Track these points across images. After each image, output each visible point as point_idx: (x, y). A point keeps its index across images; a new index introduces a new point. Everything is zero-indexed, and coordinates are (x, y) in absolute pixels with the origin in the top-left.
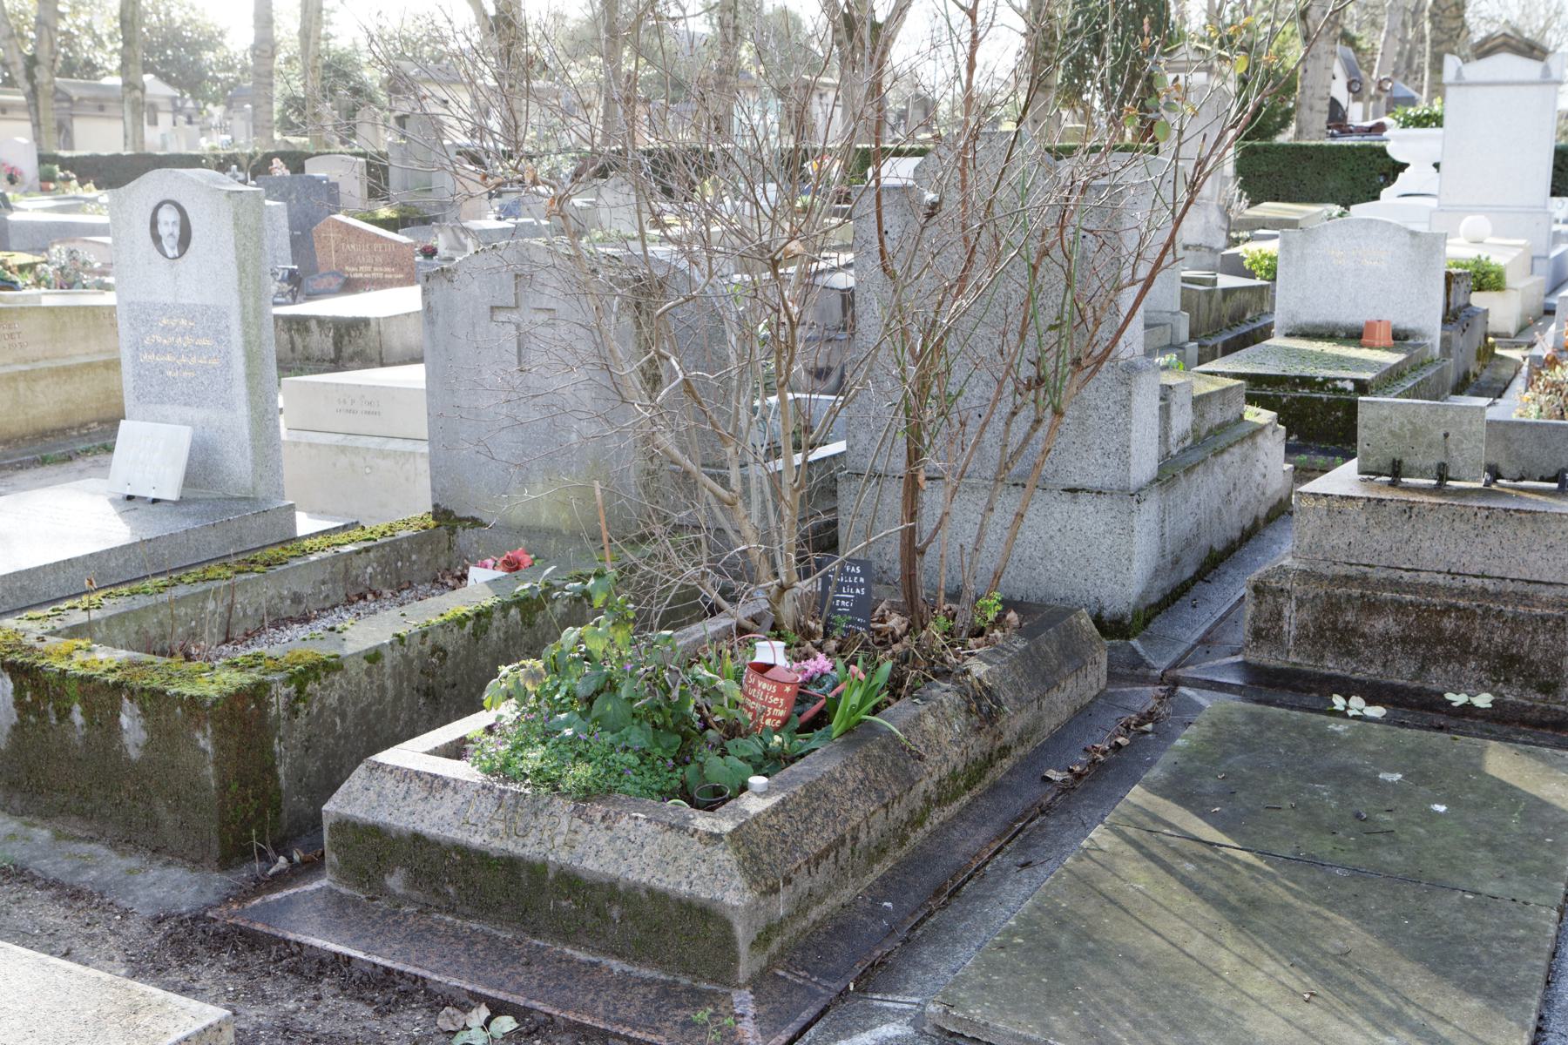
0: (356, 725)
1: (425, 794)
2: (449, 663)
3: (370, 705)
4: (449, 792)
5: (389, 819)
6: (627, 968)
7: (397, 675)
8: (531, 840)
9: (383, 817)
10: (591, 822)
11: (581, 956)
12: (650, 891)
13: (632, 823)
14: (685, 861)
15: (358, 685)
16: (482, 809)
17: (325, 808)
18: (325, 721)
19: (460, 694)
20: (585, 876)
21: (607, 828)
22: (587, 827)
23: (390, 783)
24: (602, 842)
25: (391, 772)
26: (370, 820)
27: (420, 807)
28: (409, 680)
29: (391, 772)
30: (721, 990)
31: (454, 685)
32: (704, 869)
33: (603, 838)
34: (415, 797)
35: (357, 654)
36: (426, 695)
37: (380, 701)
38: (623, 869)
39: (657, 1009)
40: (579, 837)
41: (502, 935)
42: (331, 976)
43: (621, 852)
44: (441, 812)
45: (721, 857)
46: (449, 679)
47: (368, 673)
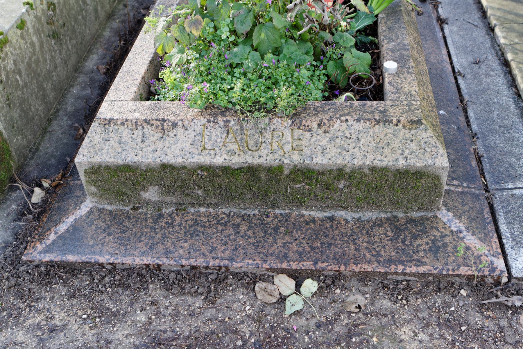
0: (28, 75)
1: (160, 135)
2: (58, 11)
3: (30, 59)
4: (180, 130)
5: (136, 159)
6: (356, 216)
7: (38, 32)
8: (264, 151)
9: (130, 158)
10: (310, 130)
11: (317, 214)
12: (373, 169)
13: (344, 125)
14: (396, 143)
15: (20, 48)
16: (214, 137)
17: (76, 160)
18: (12, 82)
19: (68, 29)
20: (317, 168)
21: (325, 132)
22: (308, 135)
23: (125, 133)
24: (324, 142)
25: (123, 124)
26: (121, 162)
27: (160, 145)
28: (43, 31)
29: (123, 124)
30: (430, 214)
31: (64, 24)
32: (413, 146)
33: (324, 140)
34: (152, 139)
35: (12, 27)
36: (54, 37)
37: (34, 53)
38: (348, 158)
39: (404, 242)
40: (304, 142)
41: (250, 212)
42: (153, 282)
43: (342, 147)
44: (179, 146)
45: (424, 136)
46: (61, 22)
47: (23, 37)
